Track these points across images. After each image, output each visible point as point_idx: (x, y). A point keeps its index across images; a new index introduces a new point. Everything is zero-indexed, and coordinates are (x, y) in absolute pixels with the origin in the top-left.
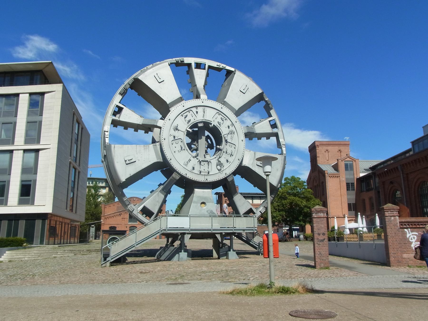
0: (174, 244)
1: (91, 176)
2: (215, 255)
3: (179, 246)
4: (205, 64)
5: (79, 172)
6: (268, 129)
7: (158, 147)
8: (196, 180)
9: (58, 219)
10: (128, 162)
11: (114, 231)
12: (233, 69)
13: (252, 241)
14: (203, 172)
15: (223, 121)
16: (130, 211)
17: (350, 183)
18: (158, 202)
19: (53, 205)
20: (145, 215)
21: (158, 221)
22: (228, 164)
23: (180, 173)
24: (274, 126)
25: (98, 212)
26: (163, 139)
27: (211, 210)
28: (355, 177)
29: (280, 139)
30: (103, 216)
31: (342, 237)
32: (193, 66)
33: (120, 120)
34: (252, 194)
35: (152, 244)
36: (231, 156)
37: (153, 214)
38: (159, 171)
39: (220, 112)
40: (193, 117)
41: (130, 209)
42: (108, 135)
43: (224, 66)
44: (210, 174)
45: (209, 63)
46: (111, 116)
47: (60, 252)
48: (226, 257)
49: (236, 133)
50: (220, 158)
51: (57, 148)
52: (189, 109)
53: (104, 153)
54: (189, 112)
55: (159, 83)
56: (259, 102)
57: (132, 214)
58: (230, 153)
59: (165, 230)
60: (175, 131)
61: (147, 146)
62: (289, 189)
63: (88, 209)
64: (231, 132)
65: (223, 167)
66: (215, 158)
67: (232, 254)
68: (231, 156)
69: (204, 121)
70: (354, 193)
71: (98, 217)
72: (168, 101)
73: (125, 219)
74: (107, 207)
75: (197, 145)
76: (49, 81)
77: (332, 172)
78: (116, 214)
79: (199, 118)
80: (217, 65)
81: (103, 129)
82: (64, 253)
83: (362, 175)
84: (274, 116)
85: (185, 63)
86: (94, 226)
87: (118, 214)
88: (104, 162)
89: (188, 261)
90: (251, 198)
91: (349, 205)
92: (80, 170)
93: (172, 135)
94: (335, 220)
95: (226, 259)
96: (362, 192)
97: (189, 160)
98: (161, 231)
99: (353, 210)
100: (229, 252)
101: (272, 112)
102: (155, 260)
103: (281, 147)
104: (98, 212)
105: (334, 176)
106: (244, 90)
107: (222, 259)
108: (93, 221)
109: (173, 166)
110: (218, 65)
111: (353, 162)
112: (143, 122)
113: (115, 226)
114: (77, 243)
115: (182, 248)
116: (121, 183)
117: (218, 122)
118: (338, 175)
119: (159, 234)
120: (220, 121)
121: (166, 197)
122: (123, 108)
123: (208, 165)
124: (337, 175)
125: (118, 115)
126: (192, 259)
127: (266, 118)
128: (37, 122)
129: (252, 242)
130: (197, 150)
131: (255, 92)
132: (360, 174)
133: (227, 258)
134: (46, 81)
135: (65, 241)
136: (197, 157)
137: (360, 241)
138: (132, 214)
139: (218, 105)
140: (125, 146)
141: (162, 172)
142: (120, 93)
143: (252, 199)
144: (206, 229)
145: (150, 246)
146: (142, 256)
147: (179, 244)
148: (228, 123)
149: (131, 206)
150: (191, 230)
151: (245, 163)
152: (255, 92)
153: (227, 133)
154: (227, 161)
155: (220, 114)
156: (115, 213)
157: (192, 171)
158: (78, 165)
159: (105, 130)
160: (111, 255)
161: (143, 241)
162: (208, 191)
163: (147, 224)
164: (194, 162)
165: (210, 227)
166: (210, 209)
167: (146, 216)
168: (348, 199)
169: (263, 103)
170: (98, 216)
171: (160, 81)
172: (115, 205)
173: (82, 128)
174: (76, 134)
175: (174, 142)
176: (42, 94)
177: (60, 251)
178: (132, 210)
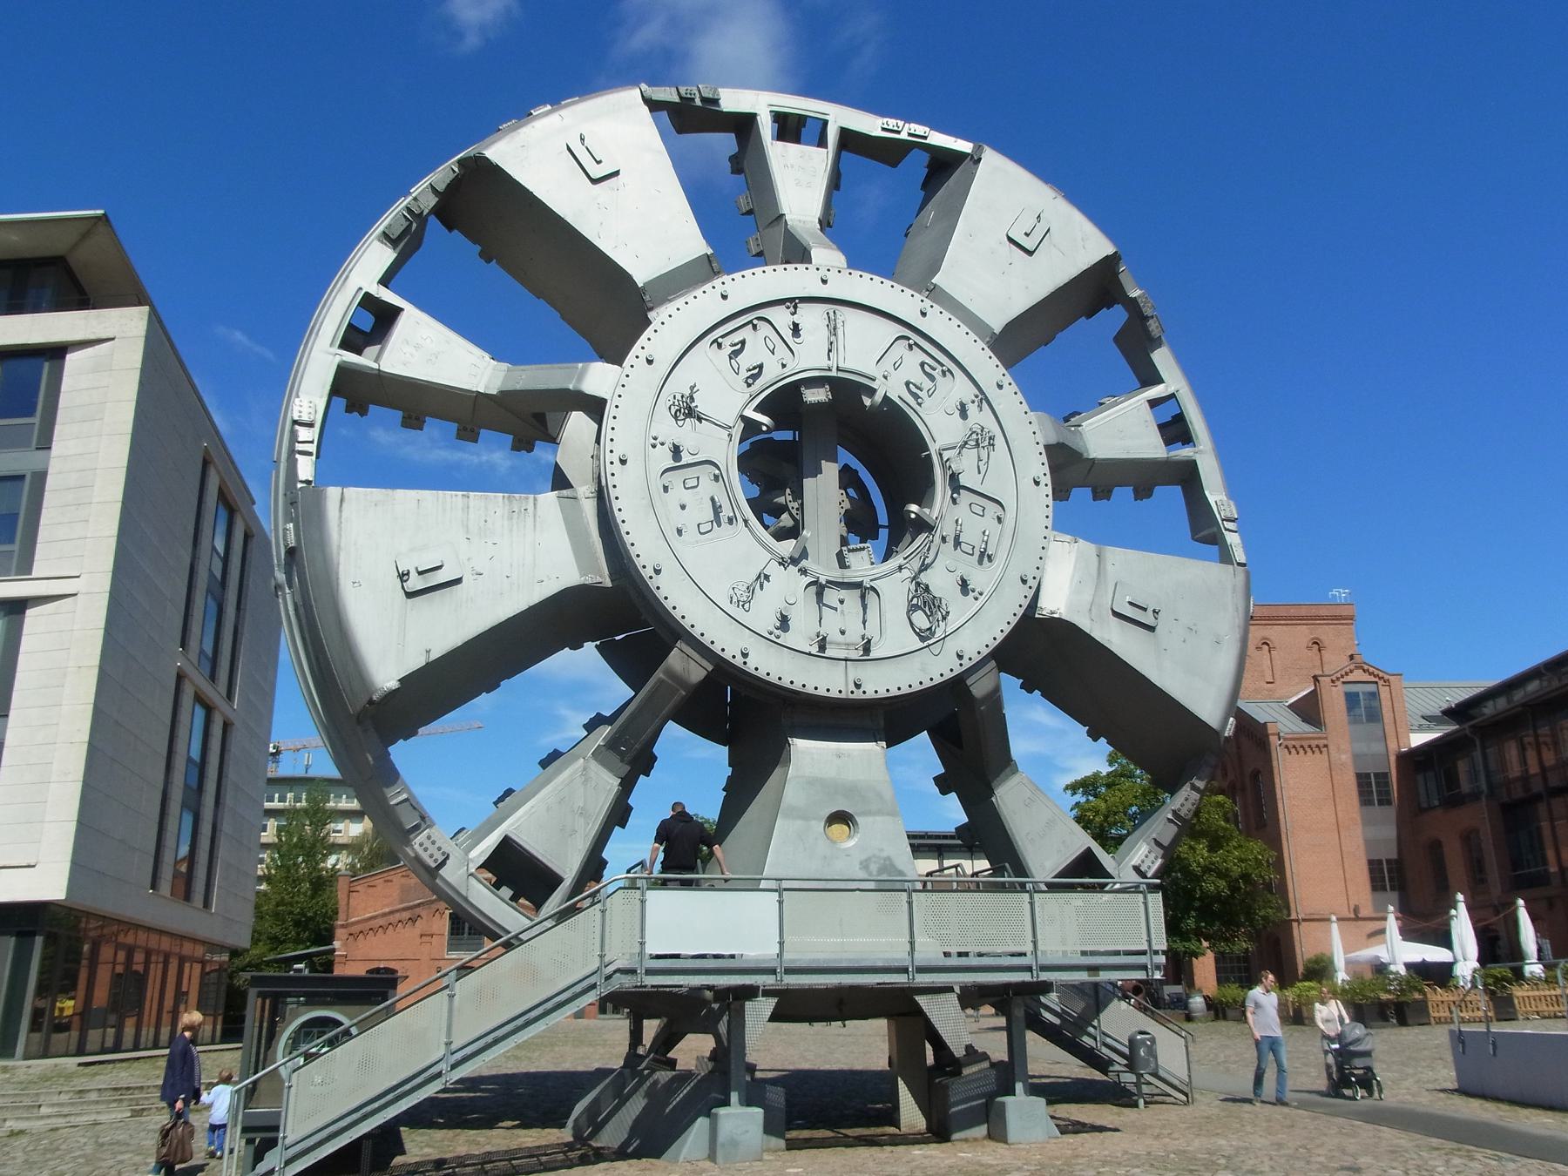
0: (670, 1055)
1: (309, 771)
2: (911, 1114)
3: (710, 1065)
4: (825, 123)
5: (227, 726)
6: (1147, 444)
7: (589, 508)
8: (797, 686)
9: (153, 942)
10: (415, 583)
11: (324, 982)
12: (965, 146)
13: (1091, 1029)
14: (839, 644)
15: (932, 378)
16: (426, 868)
17: (1372, 775)
18: (583, 812)
19: (72, 861)
20: (512, 893)
21: (589, 918)
22: (970, 605)
23: (711, 646)
24: (1175, 430)
25: (327, 912)
26: (617, 462)
27: (885, 859)
28: (1389, 749)
29: (1207, 493)
30: (343, 926)
31: (1416, 1001)
32: (766, 127)
33: (379, 370)
34: (938, 837)
35: (546, 1046)
36: (980, 562)
37: (553, 881)
38: (590, 647)
39: (912, 334)
40: (773, 353)
41: (425, 856)
42: (312, 442)
43: (920, 129)
44: (873, 655)
45: (840, 117)
46: (331, 345)
47: (53, 1105)
48: (986, 1125)
49: (999, 441)
50: (926, 569)
51: (110, 593)
52: (754, 314)
53: (285, 539)
54: (755, 327)
55: (595, 181)
56: (1089, 316)
57: (438, 881)
58: (979, 547)
59: (632, 972)
60: (680, 423)
61: (527, 498)
62: (1136, 797)
63: (283, 898)
64: (974, 436)
65: (944, 618)
66: (900, 568)
67: (1023, 1110)
68: (980, 562)
69: (834, 373)
70: (1391, 812)
71: (324, 933)
72: (641, 275)
73: (432, 936)
74: (358, 888)
75: (796, 505)
76: (89, 299)
77: (1295, 729)
78: (397, 916)
79: (810, 357)
80: (883, 129)
81: (289, 413)
82: (74, 1110)
83: (1418, 739)
84: (1173, 379)
85: (724, 110)
86: (306, 967)
87: (406, 915)
88: (287, 591)
89: (766, 1157)
90: (936, 854)
91: (1374, 867)
92: (232, 716)
93: (662, 444)
94: (1335, 927)
95: (984, 1138)
96: (1422, 811)
97: (759, 576)
98: (608, 978)
99: (1392, 889)
100: (1008, 1099)
101: (1162, 358)
102: (565, 1153)
103: (1215, 529)
104: (327, 912)
105: (1305, 744)
106: (1027, 235)
107: (966, 1140)
108: (301, 946)
109: (668, 605)
110: (891, 127)
111: (1380, 687)
112: (506, 378)
113: (392, 965)
114: (213, 1043)
115: (733, 1083)
116: (375, 698)
117: (908, 384)
118: (1321, 743)
119: (592, 997)
120: (918, 377)
121: (627, 785)
122: (402, 310)
123: (865, 607)
124: (1316, 742)
125: (372, 351)
126: (792, 1145)
127: (1130, 392)
128: (21, 478)
129: (1090, 1035)
130: (793, 532)
131: (1084, 248)
132: (1411, 734)
133: (998, 1133)
134: (77, 296)
135: (147, 1033)
136: (804, 563)
137: (1461, 1025)
138: (438, 881)
139: (902, 300)
140: (400, 494)
141: (606, 651)
142: (384, 232)
143: (939, 856)
144: (880, 964)
145: (537, 1054)
146: (489, 1123)
147: (708, 1054)
148: (960, 389)
149: (429, 837)
150: (789, 971)
151: (1054, 603)
152: (1084, 248)
153: (958, 439)
154: (964, 586)
155: (916, 344)
156: (391, 913)
157: (778, 637)
158: (224, 692)
159: (296, 418)
160: (284, 1138)
161: (496, 1042)
162: (865, 750)
163: (516, 937)
164: (788, 586)
165: (899, 955)
166: (882, 850)
167: (514, 898)
168: (1368, 843)
169: (1114, 317)
170: (326, 929)
171: (596, 172)
172: (391, 881)
173: (247, 537)
174: (219, 556)
175: (675, 478)
176: (56, 353)
177: (55, 1099)
178: (436, 861)
